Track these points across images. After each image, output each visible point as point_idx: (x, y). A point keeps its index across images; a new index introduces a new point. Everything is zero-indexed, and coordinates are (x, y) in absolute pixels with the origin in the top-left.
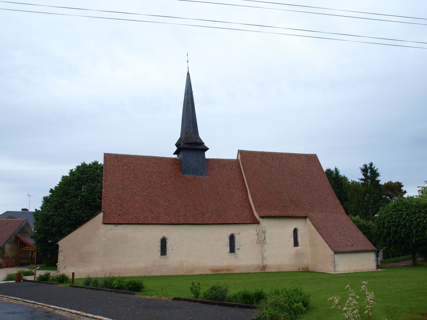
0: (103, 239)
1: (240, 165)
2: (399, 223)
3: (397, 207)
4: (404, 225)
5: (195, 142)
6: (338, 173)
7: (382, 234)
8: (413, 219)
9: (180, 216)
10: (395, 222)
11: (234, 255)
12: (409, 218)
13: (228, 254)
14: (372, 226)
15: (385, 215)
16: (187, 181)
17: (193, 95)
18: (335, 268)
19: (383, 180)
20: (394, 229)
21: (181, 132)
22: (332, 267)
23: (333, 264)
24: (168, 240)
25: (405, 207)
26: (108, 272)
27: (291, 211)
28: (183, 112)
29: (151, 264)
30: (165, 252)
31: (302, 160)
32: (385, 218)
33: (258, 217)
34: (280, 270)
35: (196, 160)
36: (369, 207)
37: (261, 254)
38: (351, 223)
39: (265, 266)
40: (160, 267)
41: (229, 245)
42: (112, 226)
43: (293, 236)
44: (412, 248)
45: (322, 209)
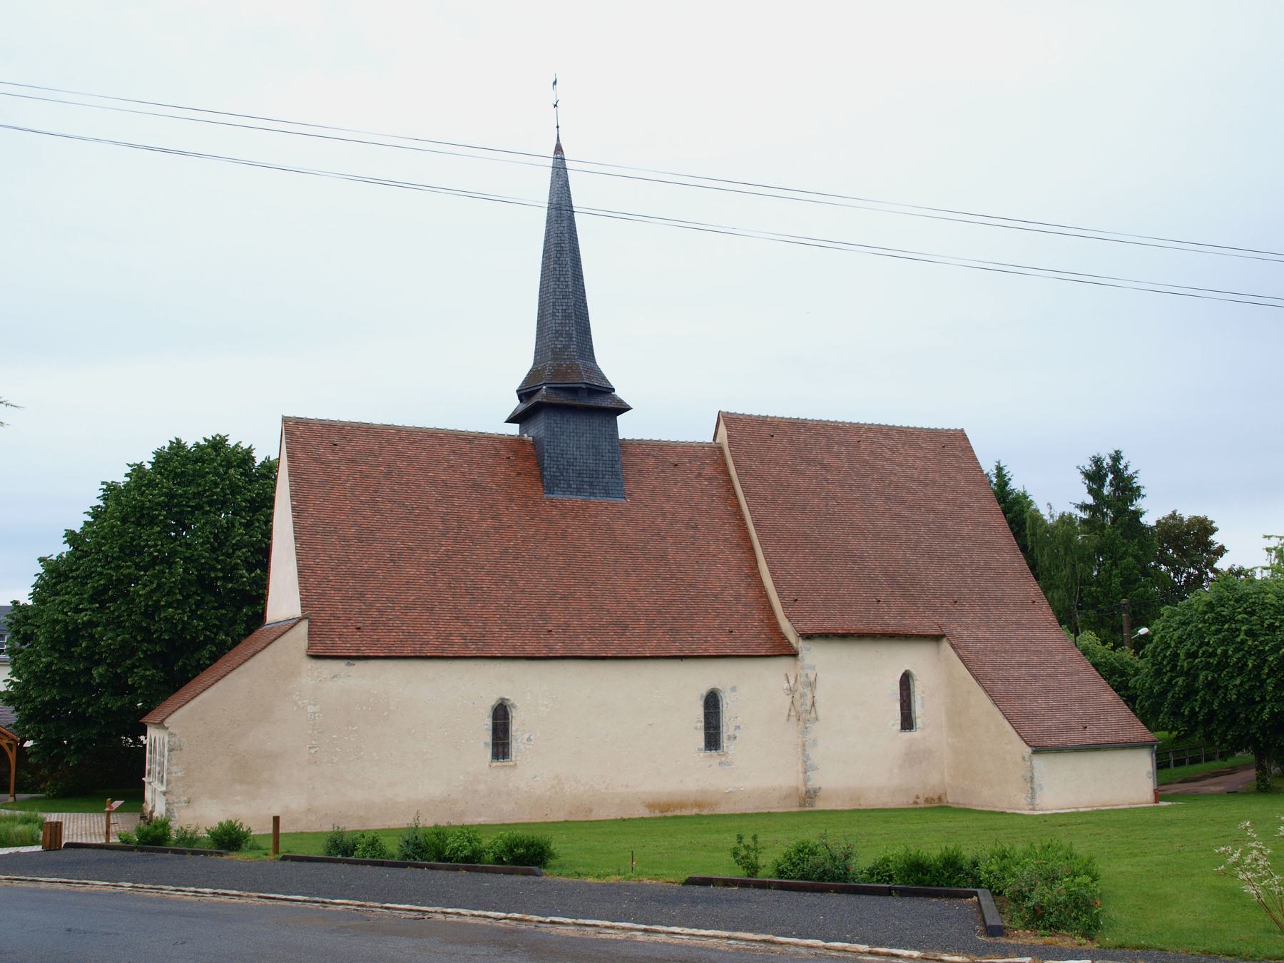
0: (310, 709)
1: (725, 464)
2: (1224, 660)
3: (1219, 609)
4: (1240, 665)
5: (588, 386)
6: (1006, 484)
7: (1169, 691)
8: (1267, 648)
9: (551, 631)
10: (1213, 655)
11: (719, 757)
12: (1256, 643)
13: (701, 755)
14: (1132, 666)
15: (1179, 632)
16: (564, 517)
17: (575, 225)
18: (1033, 798)
19: (1152, 512)
20: (1210, 678)
21: (536, 349)
22: (1024, 795)
23: (1029, 785)
24: (513, 710)
25: (1242, 608)
26: (326, 814)
27: (895, 618)
28: (541, 282)
29: (461, 788)
30: (506, 750)
31: (921, 448)
32: (1181, 643)
33: (792, 637)
34: (860, 805)
35: (591, 446)
36: (1121, 605)
37: (800, 754)
38: (1077, 656)
39: (815, 792)
40: (492, 795)
41: (703, 724)
42: (340, 666)
43: (899, 698)
44: (1259, 735)
45: (989, 610)
